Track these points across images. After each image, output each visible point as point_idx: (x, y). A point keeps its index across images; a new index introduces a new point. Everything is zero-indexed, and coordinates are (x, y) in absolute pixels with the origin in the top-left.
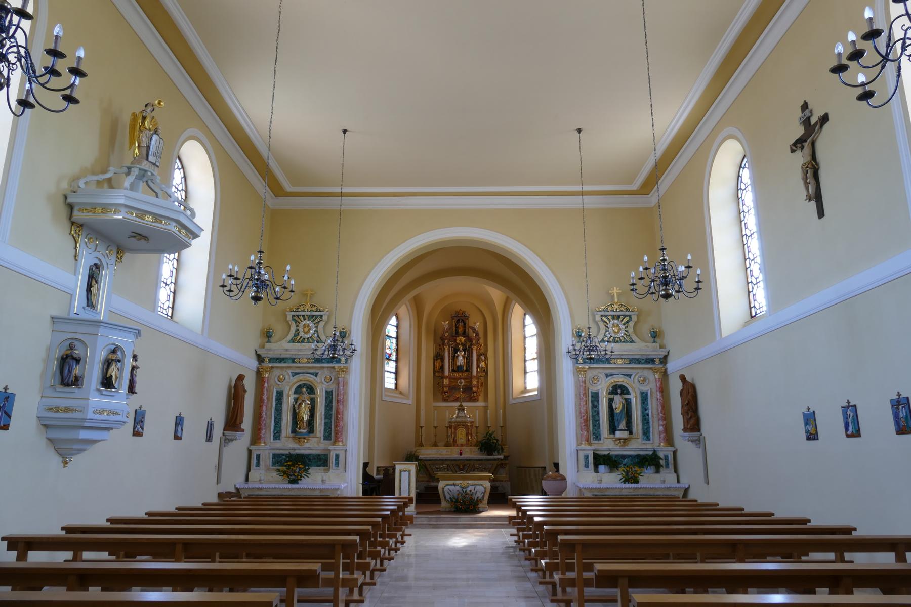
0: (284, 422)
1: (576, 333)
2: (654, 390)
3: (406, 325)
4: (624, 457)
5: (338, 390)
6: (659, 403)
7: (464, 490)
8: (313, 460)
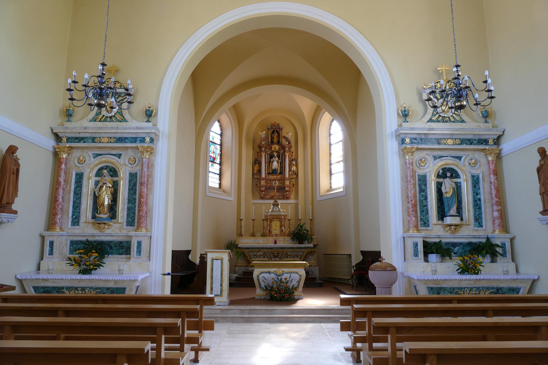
0: (83, 207)
2: (486, 173)
3: (228, 133)
4: (454, 245)
6: (493, 187)
7: (280, 278)
8: (114, 247)
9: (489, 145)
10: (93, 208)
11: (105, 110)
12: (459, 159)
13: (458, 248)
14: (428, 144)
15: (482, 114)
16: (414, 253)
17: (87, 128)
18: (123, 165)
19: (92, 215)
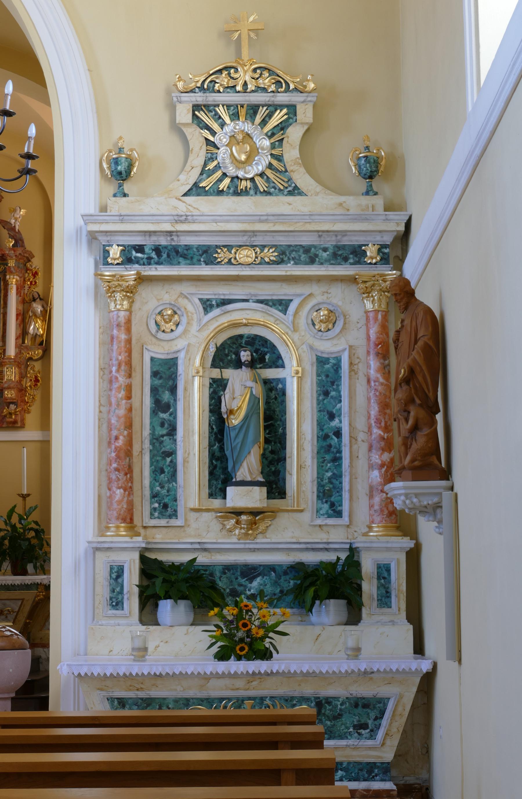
1: (109, 163)
2: (361, 352)
9: (366, 263)
12: (280, 308)
13: (262, 582)
14: (179, 263)
15: (359, 167)
16: (111, 599)
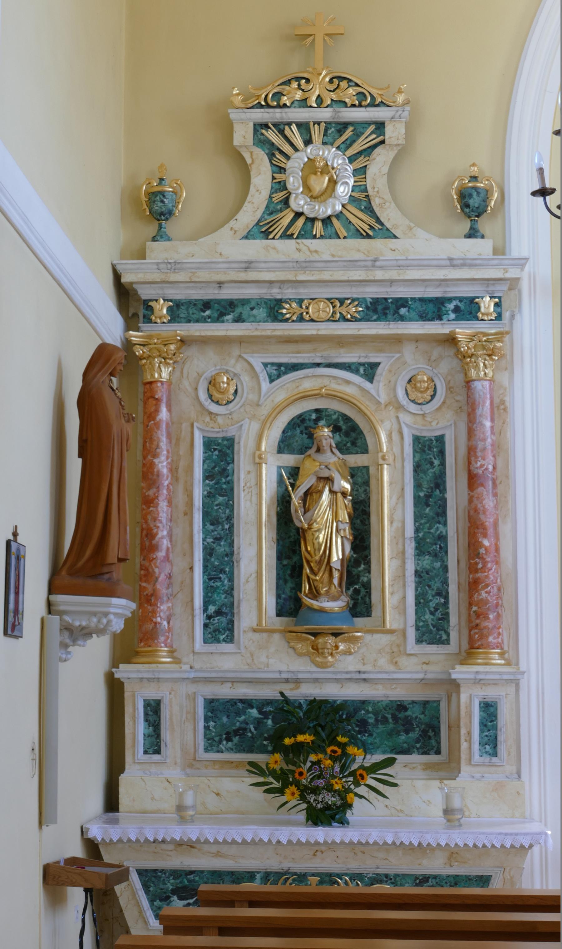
5: (471, 433)
10: (278, 574)
11: (302, 193)
17: (253, 265)
18: (386, 406)
19: (277, 603)
